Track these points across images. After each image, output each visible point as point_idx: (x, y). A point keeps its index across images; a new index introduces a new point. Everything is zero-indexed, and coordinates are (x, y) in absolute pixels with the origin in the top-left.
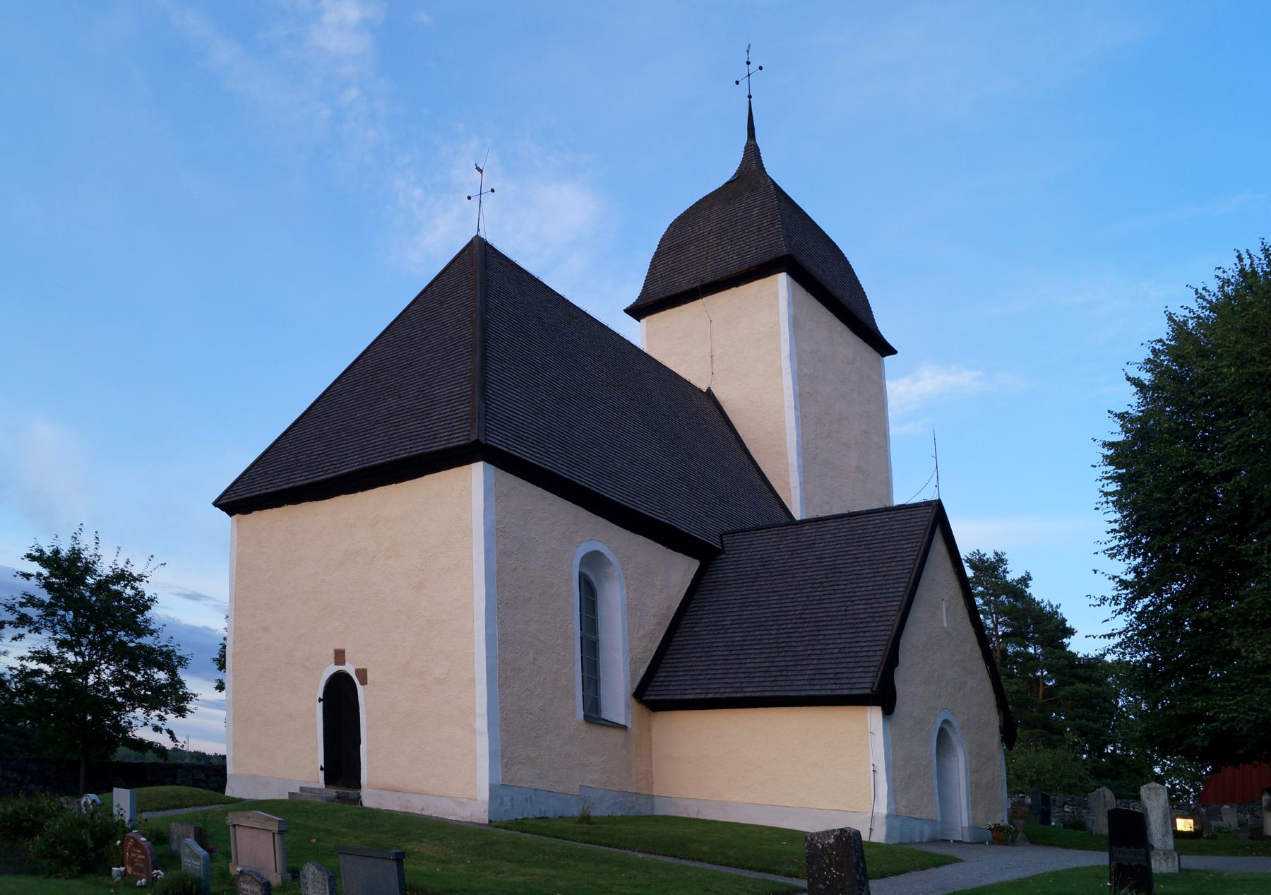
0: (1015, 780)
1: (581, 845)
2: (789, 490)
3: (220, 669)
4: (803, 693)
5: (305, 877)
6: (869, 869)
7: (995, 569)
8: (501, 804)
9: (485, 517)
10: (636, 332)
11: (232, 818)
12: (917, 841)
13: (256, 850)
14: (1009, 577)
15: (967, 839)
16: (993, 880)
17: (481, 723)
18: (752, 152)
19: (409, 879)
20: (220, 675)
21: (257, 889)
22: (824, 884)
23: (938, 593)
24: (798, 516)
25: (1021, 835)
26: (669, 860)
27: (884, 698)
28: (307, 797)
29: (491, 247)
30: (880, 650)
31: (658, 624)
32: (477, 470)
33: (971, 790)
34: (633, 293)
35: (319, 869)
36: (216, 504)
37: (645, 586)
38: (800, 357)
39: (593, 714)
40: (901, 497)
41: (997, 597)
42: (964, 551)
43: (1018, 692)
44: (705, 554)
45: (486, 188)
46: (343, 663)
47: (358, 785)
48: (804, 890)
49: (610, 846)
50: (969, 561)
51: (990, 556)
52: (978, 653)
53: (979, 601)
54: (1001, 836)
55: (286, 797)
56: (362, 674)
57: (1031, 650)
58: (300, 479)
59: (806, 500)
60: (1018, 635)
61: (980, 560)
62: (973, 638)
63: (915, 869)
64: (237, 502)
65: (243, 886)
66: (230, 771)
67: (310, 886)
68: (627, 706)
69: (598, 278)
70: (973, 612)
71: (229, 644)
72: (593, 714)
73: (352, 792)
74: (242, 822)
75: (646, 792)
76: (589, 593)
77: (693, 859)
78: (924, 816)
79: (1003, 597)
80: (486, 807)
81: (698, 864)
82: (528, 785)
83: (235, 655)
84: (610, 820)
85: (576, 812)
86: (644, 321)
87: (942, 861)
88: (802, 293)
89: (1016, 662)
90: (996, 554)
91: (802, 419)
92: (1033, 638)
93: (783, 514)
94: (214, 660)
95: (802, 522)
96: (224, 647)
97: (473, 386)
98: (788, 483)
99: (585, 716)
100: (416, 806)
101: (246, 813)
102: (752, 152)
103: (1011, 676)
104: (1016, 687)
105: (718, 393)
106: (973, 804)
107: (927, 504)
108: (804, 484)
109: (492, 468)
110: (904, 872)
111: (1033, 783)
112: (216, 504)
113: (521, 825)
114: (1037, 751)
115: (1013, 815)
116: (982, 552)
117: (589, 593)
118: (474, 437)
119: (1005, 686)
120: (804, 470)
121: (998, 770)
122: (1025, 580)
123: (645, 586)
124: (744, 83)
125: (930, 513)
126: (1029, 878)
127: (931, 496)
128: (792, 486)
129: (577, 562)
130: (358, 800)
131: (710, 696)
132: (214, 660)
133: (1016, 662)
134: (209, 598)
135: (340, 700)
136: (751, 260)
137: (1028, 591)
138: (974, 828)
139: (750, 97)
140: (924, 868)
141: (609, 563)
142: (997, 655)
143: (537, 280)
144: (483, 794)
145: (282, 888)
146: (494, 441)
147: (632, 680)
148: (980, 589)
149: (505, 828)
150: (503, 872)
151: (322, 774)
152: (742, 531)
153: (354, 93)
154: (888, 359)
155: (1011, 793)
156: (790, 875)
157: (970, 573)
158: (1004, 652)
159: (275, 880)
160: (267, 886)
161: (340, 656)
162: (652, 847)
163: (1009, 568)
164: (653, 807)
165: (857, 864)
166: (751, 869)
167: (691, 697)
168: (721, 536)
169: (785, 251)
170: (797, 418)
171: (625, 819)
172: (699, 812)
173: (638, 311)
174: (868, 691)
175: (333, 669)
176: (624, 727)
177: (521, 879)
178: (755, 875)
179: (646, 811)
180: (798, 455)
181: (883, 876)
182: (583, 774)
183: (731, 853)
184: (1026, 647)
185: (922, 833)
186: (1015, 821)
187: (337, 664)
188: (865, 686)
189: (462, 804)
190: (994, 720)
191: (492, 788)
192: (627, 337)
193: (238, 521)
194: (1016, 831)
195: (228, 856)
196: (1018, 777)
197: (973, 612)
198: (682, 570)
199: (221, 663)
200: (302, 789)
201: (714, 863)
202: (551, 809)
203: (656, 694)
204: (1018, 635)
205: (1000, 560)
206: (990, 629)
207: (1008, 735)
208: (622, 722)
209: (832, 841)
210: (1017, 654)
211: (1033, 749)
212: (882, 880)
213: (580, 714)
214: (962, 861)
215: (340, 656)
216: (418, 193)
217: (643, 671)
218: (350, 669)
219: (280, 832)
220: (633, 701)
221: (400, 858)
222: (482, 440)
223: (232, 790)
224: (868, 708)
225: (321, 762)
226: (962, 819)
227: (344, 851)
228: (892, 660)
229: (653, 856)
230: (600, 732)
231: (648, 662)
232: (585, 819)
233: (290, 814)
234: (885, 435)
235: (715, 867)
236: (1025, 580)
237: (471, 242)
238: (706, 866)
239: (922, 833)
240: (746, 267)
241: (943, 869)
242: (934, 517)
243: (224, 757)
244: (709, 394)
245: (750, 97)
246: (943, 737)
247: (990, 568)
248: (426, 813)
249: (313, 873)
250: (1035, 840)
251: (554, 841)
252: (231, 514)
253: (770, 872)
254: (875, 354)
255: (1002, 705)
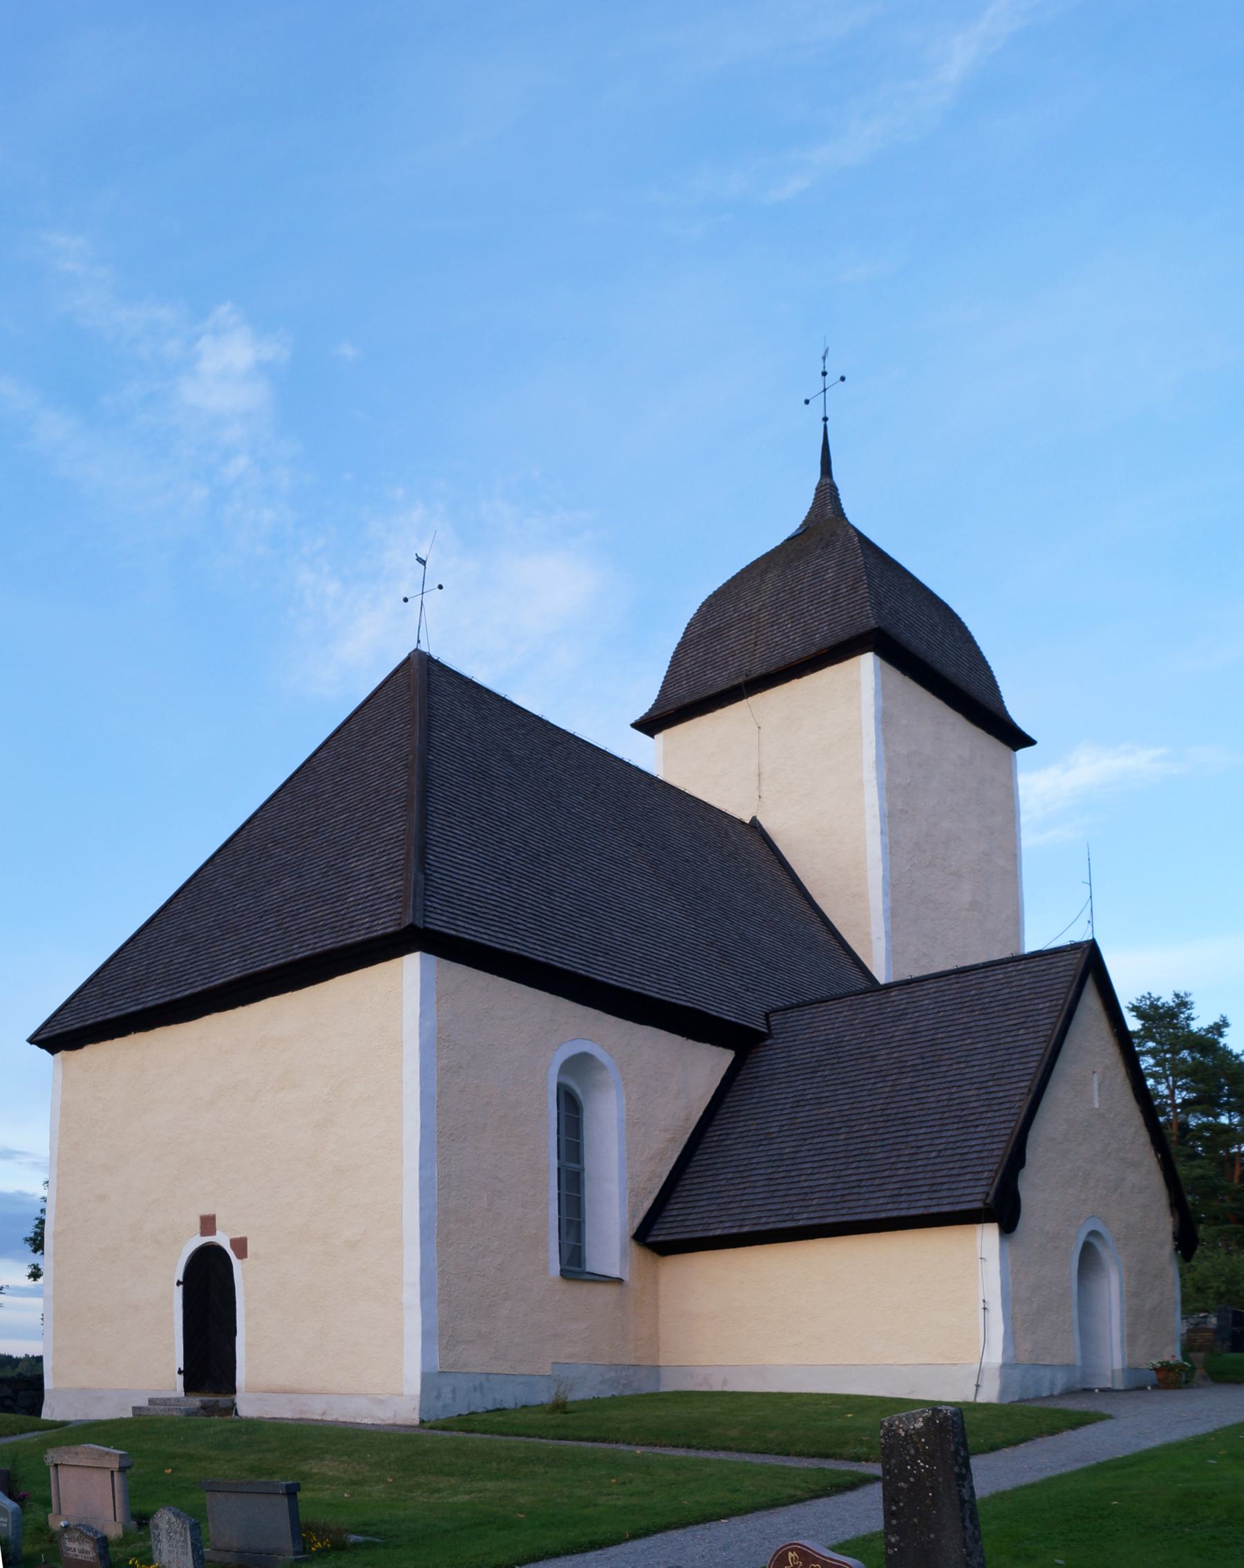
0: (1194, 1297)
1: (553, 1444)
2: (870, 942)
3: (35, 1251)
4: (883, 1215)
5: (157, 1527)
6: (971, 1441)
7: (1175, 1016)
8: (438, 1397)
9: (421, 1024)
10: (647, 754)
11: (52, 1456)
12: (1045, 1395)
13: (86, 1495)
14: (1195, 1026)
15: (1119, 1386)
16: (1156, 1441)
17: (411, 1294)
18: (827, 494)
19: (305, 1515)
20: (36, 1258)
21: (88, 1547)
22: (906, 1481)
23: (1090, 1046)
24: (882, 979)
25: (1199, 1372)
26: (681, 1453)
27: (1003, 1211)
28: (159, 1410)
29: (437, 662)
30: (999, 1149)
31: (672, 1140)
32: (410, 968)
33: (1128, 1315)
34: (644, 700)
35: (177, 1515)
36: (32, 1040)
37: (653, 1089)
38: (889, 764)
39: (574, 1265)
40: (1035, 939)
41: (1177, 1052)
42: (1126, 995)
43: (1203, 1177)
44: (741, 1040)
45: (414, 604)
46: (213, 1233)
47: (232, 1390)
48: (877, 1479)
49: (595, 1440)
50: (1134, 1008)
51: (1168, 999)
52: (1144, 1137)
53: (1147, 1062)
54: (1169, 1378)
55: (129, 1414)
56: (240, 1246)
57: (1224, 1120)
58: (152, 998)
59: (894, 953)
60: (1206, 1102)
61: (1153, 1006)
62: (1138, 1119)
63: (1041, 1434)
64: (59, 1036)
65: (69, 1544)
66: (48, 1384)
67: (164, 1538)
68: (624, 1253)
69: (594, 691)
70: (1137, 1077)
71: (49, 1219)
72: (574, 1265)
73: (222, 1400)
74: (67, 1459)
75: (649, 1363)
76: (571, 1108)
77: (716, 1449)
78: (1056, 1362)
79: (1185, 1054)
80: (416, 1403)
81: (722, 1455)
82: (477, 1370)
83: (56, 1235)
84: (596, 1404)
85: (545, 1397)
86: (659, 737)
87: (1080, 1421)
88: (897, 678)
89: (1201, 1138)
90: (1177, 996)
91: (892, 848)
92: (1227, 1103)
93: (859, 975)
94: (27, 1240)
95: (889, 987)
96: (42, 1222)
97: (408, 853)
98: (868, 934)
99: (561, 1270)
100: (316, 1410)
101: (73, 1449)
102: (827, 494)
103: (1194, 1156)
104: (1198, 1172)
105: (768, 824)
106: (1130, 1339)
107: (1075, 947)
108: (893, 932)
109: (432, 959)
110: (1023, 1441)
111: (1220, 1295)
112: (32, 1040)
113: (466, 1423)
114: (1229, 1253)
115: (1189, 1347)
116: (1155, 995)
117: (571, 1108)
118: (407, 921)
119: (1182, 1170)
120: (894, 914)
121: (1170, 1288)
122: (1218, 1028)
123: (653, 1089)
124: (817, 404)
125: (1079, 959)
126: (1210, 1434)
127: (1079, 935)
128: (874, 937)
129: (555, 1070)
130: (232, 1408)
131: (745, 1229)
132: (27, 1240)
133: (1201, 1138)
134: (24, 1153)
135: (209, 1286)
136: (823, 637)
137: (1222, 1041)
138: (1130, 1370)
139: (825, 419)
140: (1054, 1431)
141: (602, 1067)
142: (1172, 1133)
143: (503, 699)
144: (412, 1385)
145: (124, 1541)
146: (437, 923)
147: (633, 1216)
148: (1151, 1044)
149: (444, 1429)
150: (439, 1490)
151: (180, 1379)
152: (798, 1006)
153: (241, 463)
154: (1023, 754)
155: (1187, 1313)
156: (857, 1459)
157: (1133, 1024)
158: (1184, 1127)
159: (114, 1530)
160: (103, 1543)
161: (208, 1224)
162: (655, 1437)
163: (1194, 1013)
164: (658, 1380)
165: (957, 1452)
166: (800, 1454)
167: (718, 1232)
168: (767, 1016)
169: (873, 623)
170: (884, 846)
171: (617, 1402)
172: (725, 1382)
173: (650, 725)
174: (979, 1205)
175: (199, 1241)
176: (619, 1281)
177: (467, 1497)
178: (805, 1463)
179: (648, 1388)
180: (885, 894)
181: (994, 1448)
182: (555, 1346)
183: (771, 1435)
184: (1217, 1116)
185: (1053, 1384)
186: (1192, 1355)
187: (203, 1234)
188: (975, 1198)
189: (381, 1402)
190: (1164, 1225)
191: (425, 1378)
192: (634, 762)
193: (64, 1060)
194: (1193, 1369)
195: (47, 1503)
196: (1199, 1289)
197: (1137, 1077)
198: (707, 1065)
199: (37, 1243)
200: (151, 1401)
201: (747, 1451)
202: (509, 1397)
203: (667, 1230)
204: (1206, 1102)
205: (1183, 1004)
206: (1162, 1097)
207: (1186, 1243)
208: (616, 1273)
209: (920, 1425)
210: (1205, 1127)
211: (1223, 1251)
212: (992, 1455)
213: (555, 1268)
214: (1110, 1417)
215: (208, 1224)
216: (333, 588)
217: (647, 1204)
218: (222, 1239)
219: (122, 1469)
220: (633, 1248)
221: (292, 1492)
222: (420, 924)
223: (51, 1411)
224: (979, 1227)
225: (180, 1363)
226: (1114, 1359)
227: (212, 1488)
228: (1016, 1159)
229: (657, 1450)
230: (582, 1291)
231: (657, 1191)
232: (560, 1407)
233: (135, 1440)
234: (1014, 855)
235: (747, 1458)
236: (1218, 1028)
237: (408, 659)
238: (735, 1457)
239: (1053, 1384)
240: (814, 650)
241: (1083, 1432)
242: (1088, 963)
243: (39, 1360)
244: (755, 825)
245: (825, 419)
246: (1089, 1257)
247: (1165, 1018)
248: (328, 1418)
249: (169, 1522)
250: (1220, 1377)
251: (514, 1440)
252: (53, 1051)
253: (827, 1456)
254: (1002, 748)
255: (1177, 1203)
